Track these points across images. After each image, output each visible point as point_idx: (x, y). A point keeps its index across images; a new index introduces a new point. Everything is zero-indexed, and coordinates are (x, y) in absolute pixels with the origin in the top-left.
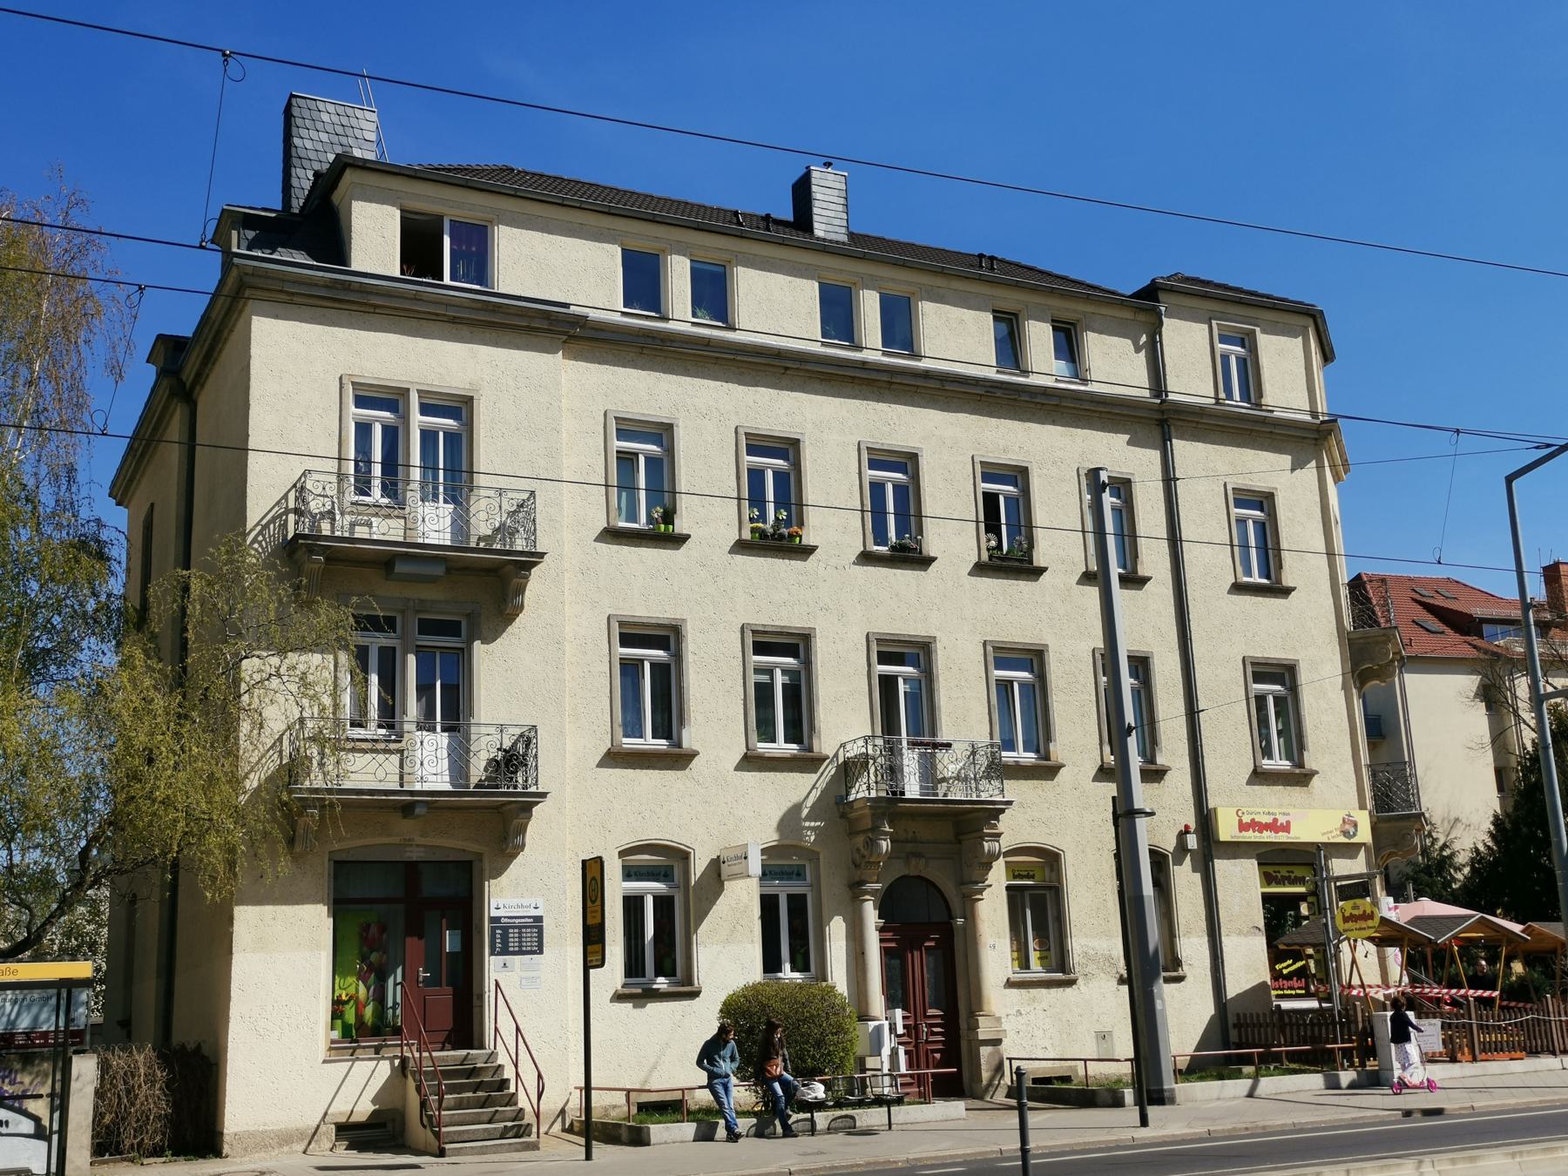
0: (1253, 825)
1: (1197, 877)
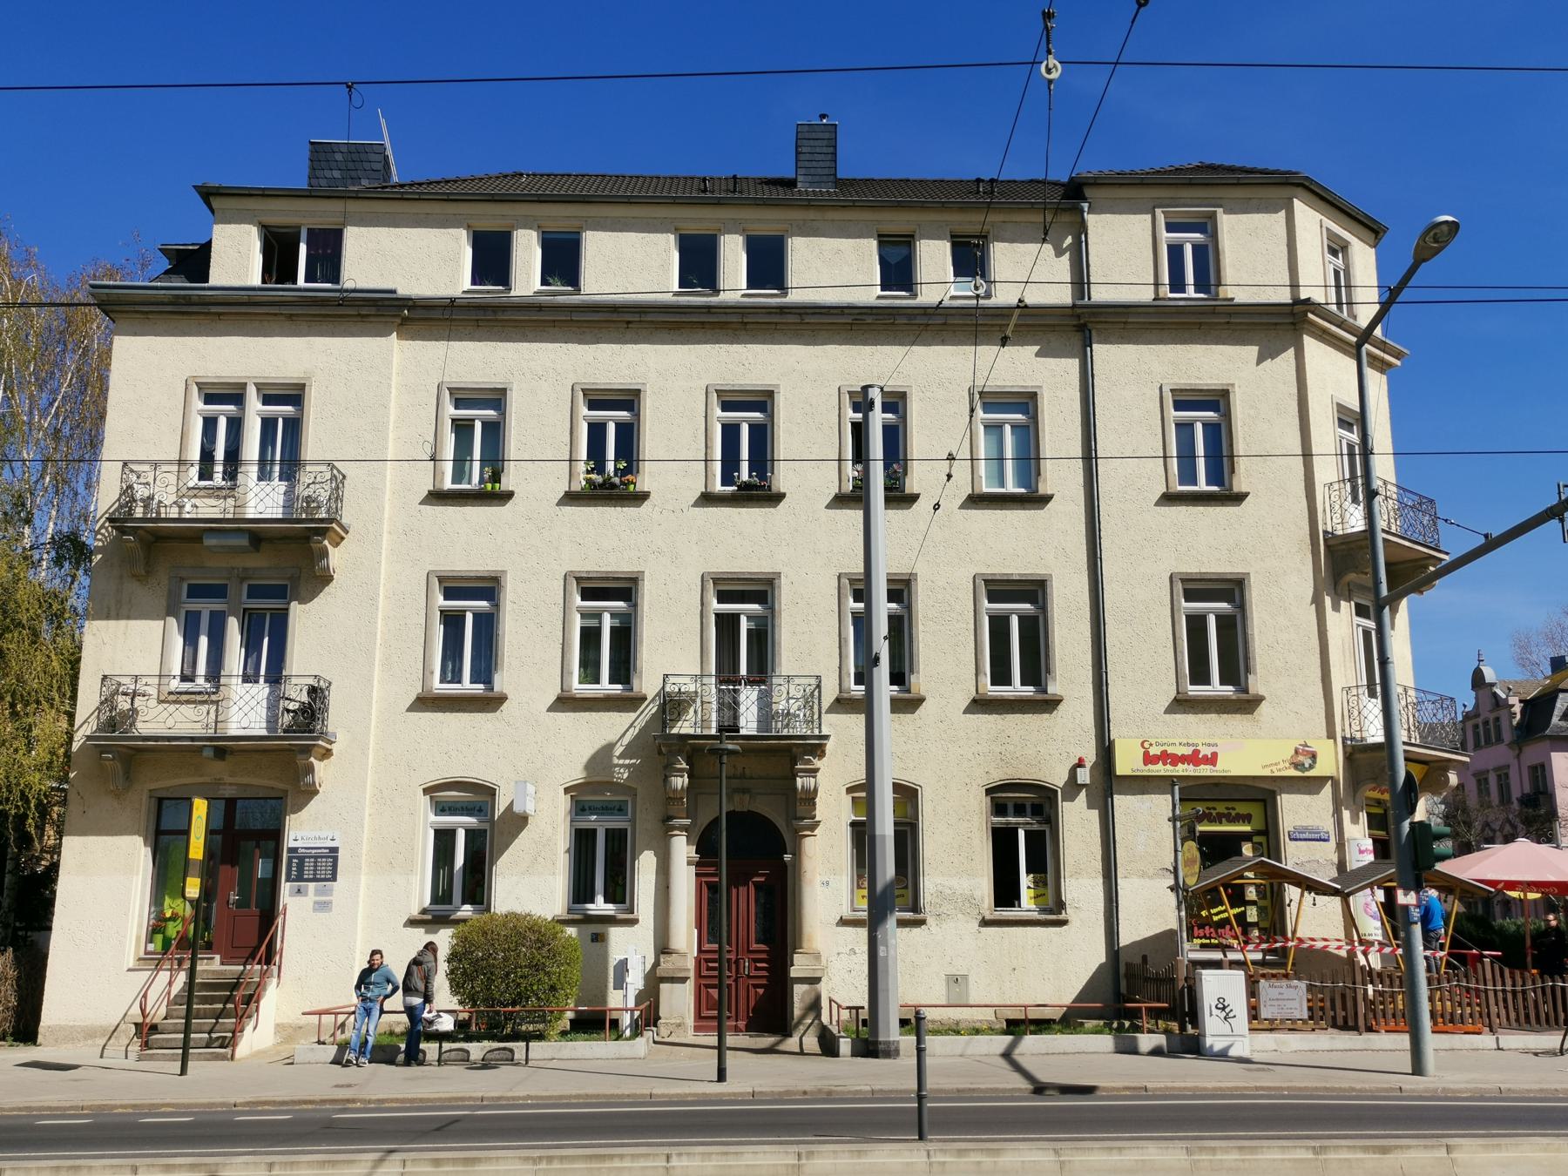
0: (1165, 757)
1: (1094, 815)
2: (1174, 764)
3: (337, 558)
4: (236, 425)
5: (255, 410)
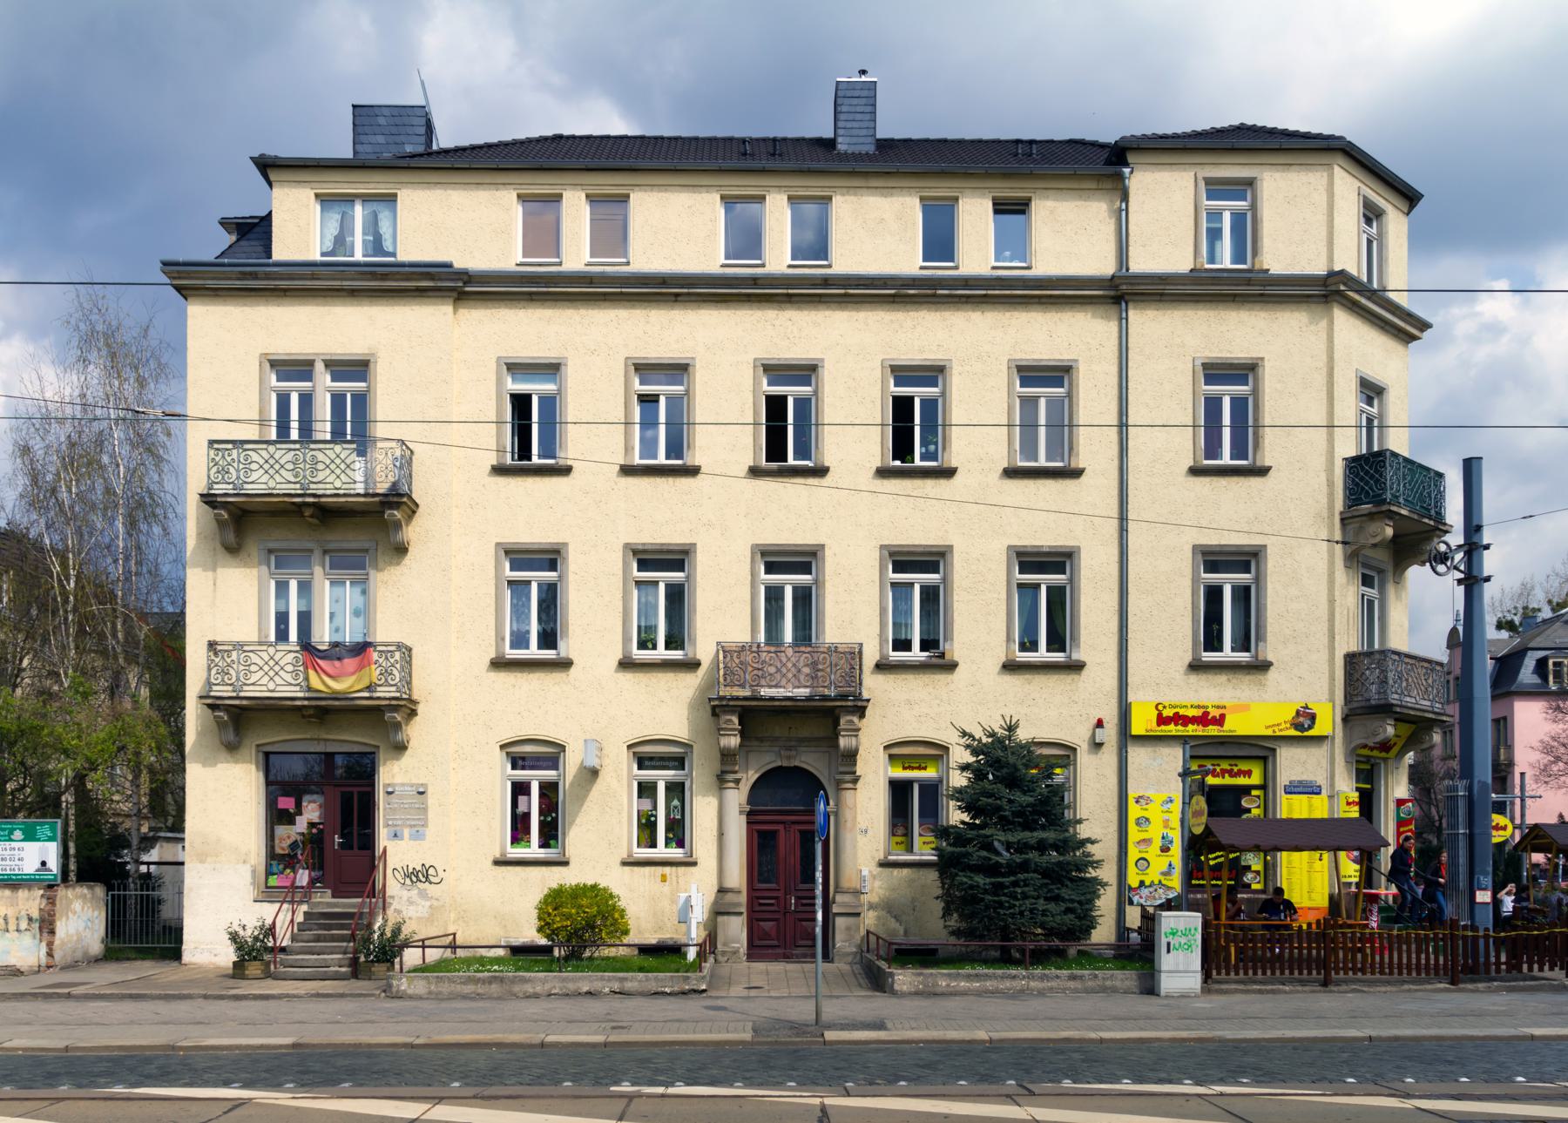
0: (1178, 719)
2: (1185, 724)
3: (413, 533)
4: (306, 400)
5: (324, 384)
